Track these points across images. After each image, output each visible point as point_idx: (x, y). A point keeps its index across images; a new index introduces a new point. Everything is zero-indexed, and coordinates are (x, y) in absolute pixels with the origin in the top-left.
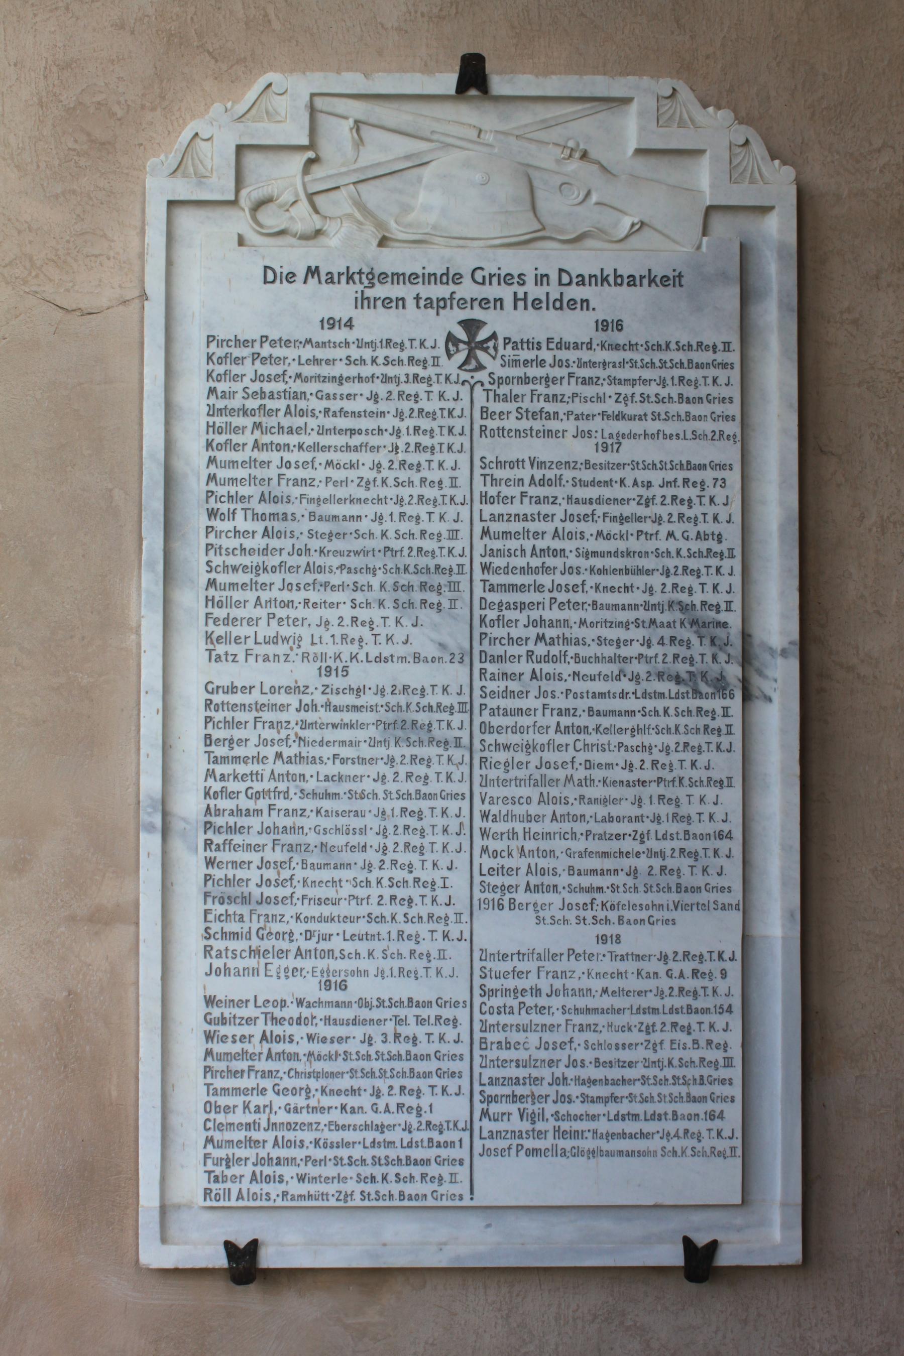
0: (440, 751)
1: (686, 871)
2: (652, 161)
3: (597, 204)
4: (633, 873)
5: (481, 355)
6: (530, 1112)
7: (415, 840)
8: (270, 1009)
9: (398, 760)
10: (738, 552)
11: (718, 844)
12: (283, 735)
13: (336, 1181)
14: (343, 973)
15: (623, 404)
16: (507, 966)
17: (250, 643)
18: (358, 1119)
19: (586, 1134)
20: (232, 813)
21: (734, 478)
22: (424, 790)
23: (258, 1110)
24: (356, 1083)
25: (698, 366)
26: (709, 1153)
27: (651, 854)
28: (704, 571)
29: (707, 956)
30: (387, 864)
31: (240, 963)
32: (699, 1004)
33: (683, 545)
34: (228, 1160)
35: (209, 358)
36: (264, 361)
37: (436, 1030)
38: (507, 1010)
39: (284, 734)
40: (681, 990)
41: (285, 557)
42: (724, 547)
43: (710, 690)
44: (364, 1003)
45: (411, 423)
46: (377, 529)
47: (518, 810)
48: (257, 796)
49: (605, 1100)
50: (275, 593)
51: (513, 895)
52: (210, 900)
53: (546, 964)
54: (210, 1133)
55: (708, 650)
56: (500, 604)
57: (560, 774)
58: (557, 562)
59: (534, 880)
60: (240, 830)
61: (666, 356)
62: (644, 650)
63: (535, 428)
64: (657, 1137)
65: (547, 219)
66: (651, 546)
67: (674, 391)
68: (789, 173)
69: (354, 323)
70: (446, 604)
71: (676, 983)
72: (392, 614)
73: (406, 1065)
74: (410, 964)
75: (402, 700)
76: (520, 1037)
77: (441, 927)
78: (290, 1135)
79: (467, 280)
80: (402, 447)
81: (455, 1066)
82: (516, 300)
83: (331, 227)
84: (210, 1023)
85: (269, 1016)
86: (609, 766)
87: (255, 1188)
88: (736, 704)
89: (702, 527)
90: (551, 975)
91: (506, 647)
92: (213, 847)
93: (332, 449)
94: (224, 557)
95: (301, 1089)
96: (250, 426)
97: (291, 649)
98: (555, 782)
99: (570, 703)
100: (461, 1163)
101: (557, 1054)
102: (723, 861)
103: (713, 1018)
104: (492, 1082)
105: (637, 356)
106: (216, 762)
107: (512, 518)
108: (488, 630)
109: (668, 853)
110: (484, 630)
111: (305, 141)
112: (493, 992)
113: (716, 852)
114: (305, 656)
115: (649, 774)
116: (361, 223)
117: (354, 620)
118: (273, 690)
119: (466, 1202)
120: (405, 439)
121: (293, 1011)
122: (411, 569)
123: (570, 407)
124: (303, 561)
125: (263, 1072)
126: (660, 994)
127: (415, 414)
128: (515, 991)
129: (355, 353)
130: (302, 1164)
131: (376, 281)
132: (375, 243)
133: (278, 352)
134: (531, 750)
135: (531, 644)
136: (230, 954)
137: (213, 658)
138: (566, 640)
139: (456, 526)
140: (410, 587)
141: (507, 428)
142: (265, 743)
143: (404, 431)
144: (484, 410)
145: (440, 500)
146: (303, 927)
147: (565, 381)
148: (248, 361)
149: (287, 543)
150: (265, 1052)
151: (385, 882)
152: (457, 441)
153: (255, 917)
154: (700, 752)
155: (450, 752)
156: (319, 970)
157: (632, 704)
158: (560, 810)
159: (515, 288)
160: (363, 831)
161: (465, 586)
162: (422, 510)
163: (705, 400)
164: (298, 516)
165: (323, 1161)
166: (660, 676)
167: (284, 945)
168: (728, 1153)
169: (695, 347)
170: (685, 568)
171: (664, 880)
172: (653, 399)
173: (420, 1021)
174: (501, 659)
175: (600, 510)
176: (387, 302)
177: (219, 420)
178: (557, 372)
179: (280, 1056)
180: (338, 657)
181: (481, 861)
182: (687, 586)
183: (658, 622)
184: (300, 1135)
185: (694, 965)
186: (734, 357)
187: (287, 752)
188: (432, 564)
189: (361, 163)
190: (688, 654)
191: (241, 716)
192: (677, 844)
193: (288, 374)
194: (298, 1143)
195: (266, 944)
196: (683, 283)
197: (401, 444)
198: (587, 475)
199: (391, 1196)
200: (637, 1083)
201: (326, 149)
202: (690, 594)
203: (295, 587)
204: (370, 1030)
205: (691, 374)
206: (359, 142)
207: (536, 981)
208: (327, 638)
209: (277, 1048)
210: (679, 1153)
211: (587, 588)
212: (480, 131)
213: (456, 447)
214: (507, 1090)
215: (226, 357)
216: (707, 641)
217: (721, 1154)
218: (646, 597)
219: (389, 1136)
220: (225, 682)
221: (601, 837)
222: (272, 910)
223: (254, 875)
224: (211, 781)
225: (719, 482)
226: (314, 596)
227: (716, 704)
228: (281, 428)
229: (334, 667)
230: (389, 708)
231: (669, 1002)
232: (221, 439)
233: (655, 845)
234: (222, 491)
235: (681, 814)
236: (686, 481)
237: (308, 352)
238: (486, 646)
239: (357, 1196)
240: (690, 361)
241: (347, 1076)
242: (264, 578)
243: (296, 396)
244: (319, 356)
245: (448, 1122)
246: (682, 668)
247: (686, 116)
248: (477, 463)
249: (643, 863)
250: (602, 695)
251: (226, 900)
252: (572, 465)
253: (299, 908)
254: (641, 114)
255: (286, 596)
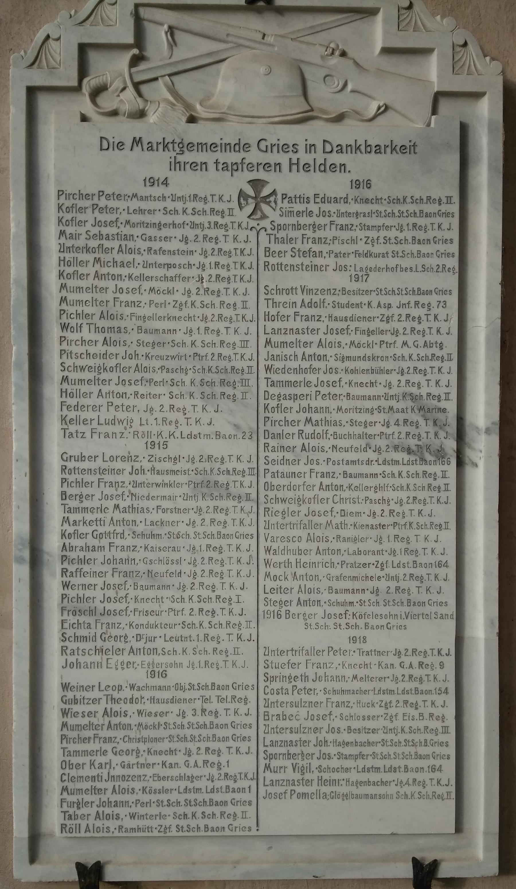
0: (235, 503)
1: (414, 590)
2: (394, 59)
3: (352, 91)
4: (376, 592)
5: (264, 207)
6: (300, 765)
7: (217, 568)
8: (110, 692)
9: (204, 510)
10: (455, 356)
11: (438, 570)
12: (120, 492)
13: (158, 818)
14: (164, 666)
15: (370, 245)
16: (284, 659)
17: (95, 423)
18: (175, 772)
19: (341, 782)
20: (82, 549)
21: (453, 300)
22: (224, 531)
23: (101, 766)
24: (173, 746)
25: (428, 215)
26: (431, 797)
27: (389, 578)
28: (429, 370)
29: (429, 652)
30: (197, 586)
31: (88, 659)
32: (424, 687)
33: (414, 351)
34: (78, 803)
35: (60, 208)
36: (101, 210)
37: (232, 706)
38: (284, 692)
39: (120, 491)
40: (411, 677)
41: (120, 360)
42: (444, 353)
43: (432, 459)
44: (179, 687)
45: (212, 259)
46: (188, 340)
47: (292, 546)
48: (101, 536)
49: (356, 758)
50: (113, 387)
51: (288, 608)
52: (65, 613)
53: (312, 658)
54: (66, 784)
55: (431, 429)
56: (279, 396)
57: (323, 520)
58: (320, 365)
59: (304, 597)
60: (87, 561)
61: (403, 208)
62: (384, 429)
63: (305, 264)
64: (393, 784)
65: (315, 104)
66: (390, 352)
67: (409, 234)
68: (497, 66)
69: (169, 182)
70: (239, 396)
71: (407, 672)
72: (199, 403)
73: (210, 732)
74: (213, 658)
75: (208, 466)
76: (293, 711)
77: (235, 631)
78: (125, 785)
79: (254, 149)
80: (206, 278)
81: (246, 732)
82: (291, 164)
83: (150, 109)
84: (66, 703)
85: (109, 697)
86: (358, 514)
87: (99, 823)
88: (452, 469)
89: (428, 338)
90: (315, 665)
91: (283, 428)
92: (68, 574)
93: (154, 279)
94: (74, 360)
95: (132, 750)
96: (92, 261)
97: (125, 428)
98: (318, 526)
99: (330, 468)
100: (250, 803)
101: (320, 724)
102: (441, 583)
103: (434, 697)
104: (273, 744)
105: (381, 208)
106: (70, 511)
107: (288, 332)
108: (270, 415)
109: (401, 577)
110: (267, 415)
111: (130, 40)
112: (274, 679)
113: (436, 577)
114: (136, 434)
115: (387, 520)
116: (174, 105)
117: (172, 407)
118: (112, 459)
119: (254, 832)
120: (208, 271)
121: (127, 693)
122: (214, 370)
123: (331, 247)
124: (133, 363)
125: (105, 738)
126: (396, 679)
127: (216, 252)
128: (290, 677)
129: (170, 205)
130: (134, 805)
131: (185, 149)
132: (184, 119)
133: (112, 204)
134: (301, 503)
135: (301, 424)
136: (80, 652)
137: (67, 435)
138: (327, 422)
139: (246, 338)
140: (213, 383)
141: (284, 263)
142: (107, 497)
143: (207, 266)
144: (267, 250)
145: (234, 318)
146: (135, 632)
147: (328, 228)
148: (89, 211)
149: (121, 350)
150: (107, 723)
151: (195, 599)
152: (247, 273)
153: (99, 625)
154: (425, 504)
155: (243, 504)
156: (146, 663)
157: (375, 469)
158: (323, 546)
159: (291, 155)
160: (179, 562)
161: (253, 382)
162: (221, 326)
163: (432, 241)
164: (129, 330)
165: (149, 804)
166: (396, 448)
167: (121, 645)
168: (445, 796)
169: (425, 201)
170: (415, 368)
171: (398, 597)
172: (393, 241)
173: (221, 700)
174: (280, 436)
175: (353, 325)
176: (194, 166)
177: (68, 256)
178: (322, 221)
179: (118, 726)
180: (160, 434)
181: (265, 583)
182: (417, 382)
183: (395, 408)
184: (132, 784)
185: (421, 658)
186: (455, 208)
187: (123, 504)
188: (229, 366)
189: (174, 59)
190: (416, 432)
191: (88, 478)
192: (408, 571)
193: (120, 220)
194: (130, 790)
195: (108, 645)
196: (417, 151)
197: (205, 275)
198: (343, 299)
199: (198, 828)
200: (379, 745)
201: (150, 51)
202: (419, 388)
203: (127, 383)
204: (183, 706)
205: (421, 221)
206: (173, 43)
207: (305, 670)
208: (151, 420)
209: (115, 720)
210: (409, 796)
211: (342, 383)
212: (264, 35)
213: (246, 278)
214: (283, 750)
215: (72, 207)
216: (430, 423)
217: (440, 797)
218: (386, 390)
219: (197, 784)
220: (76, 452)
221: (353, 565)
222: (111, 619)
223: (98, 594)
224: (66, 526)
225: (442, 304)
226: (142, 390)
227: (437, 469)
228: (115, 262)
229: (157, 442)
230: (197, 472)
231: (402, 686)
232: (70, 270)
233: (392, 572)
234: (71, 310)
235: (410, 549)
236: (417, 303)
237: (135, 204)
238: (268, 426)
239: (174, 829)
240: (421, 212)
241: (166, 741)
242: (104, 376)
243: (126, 238)
244: (143, 207)
245: (240, 774)
246: (412, 443)
247: (419, 22)
248: (262, 290)
249: (383, 585)
250: (353, 462)
251: (78, 613)
252: (332, 291)
253: (132, 618)
254: (385, 21)
255: (121, 389)
